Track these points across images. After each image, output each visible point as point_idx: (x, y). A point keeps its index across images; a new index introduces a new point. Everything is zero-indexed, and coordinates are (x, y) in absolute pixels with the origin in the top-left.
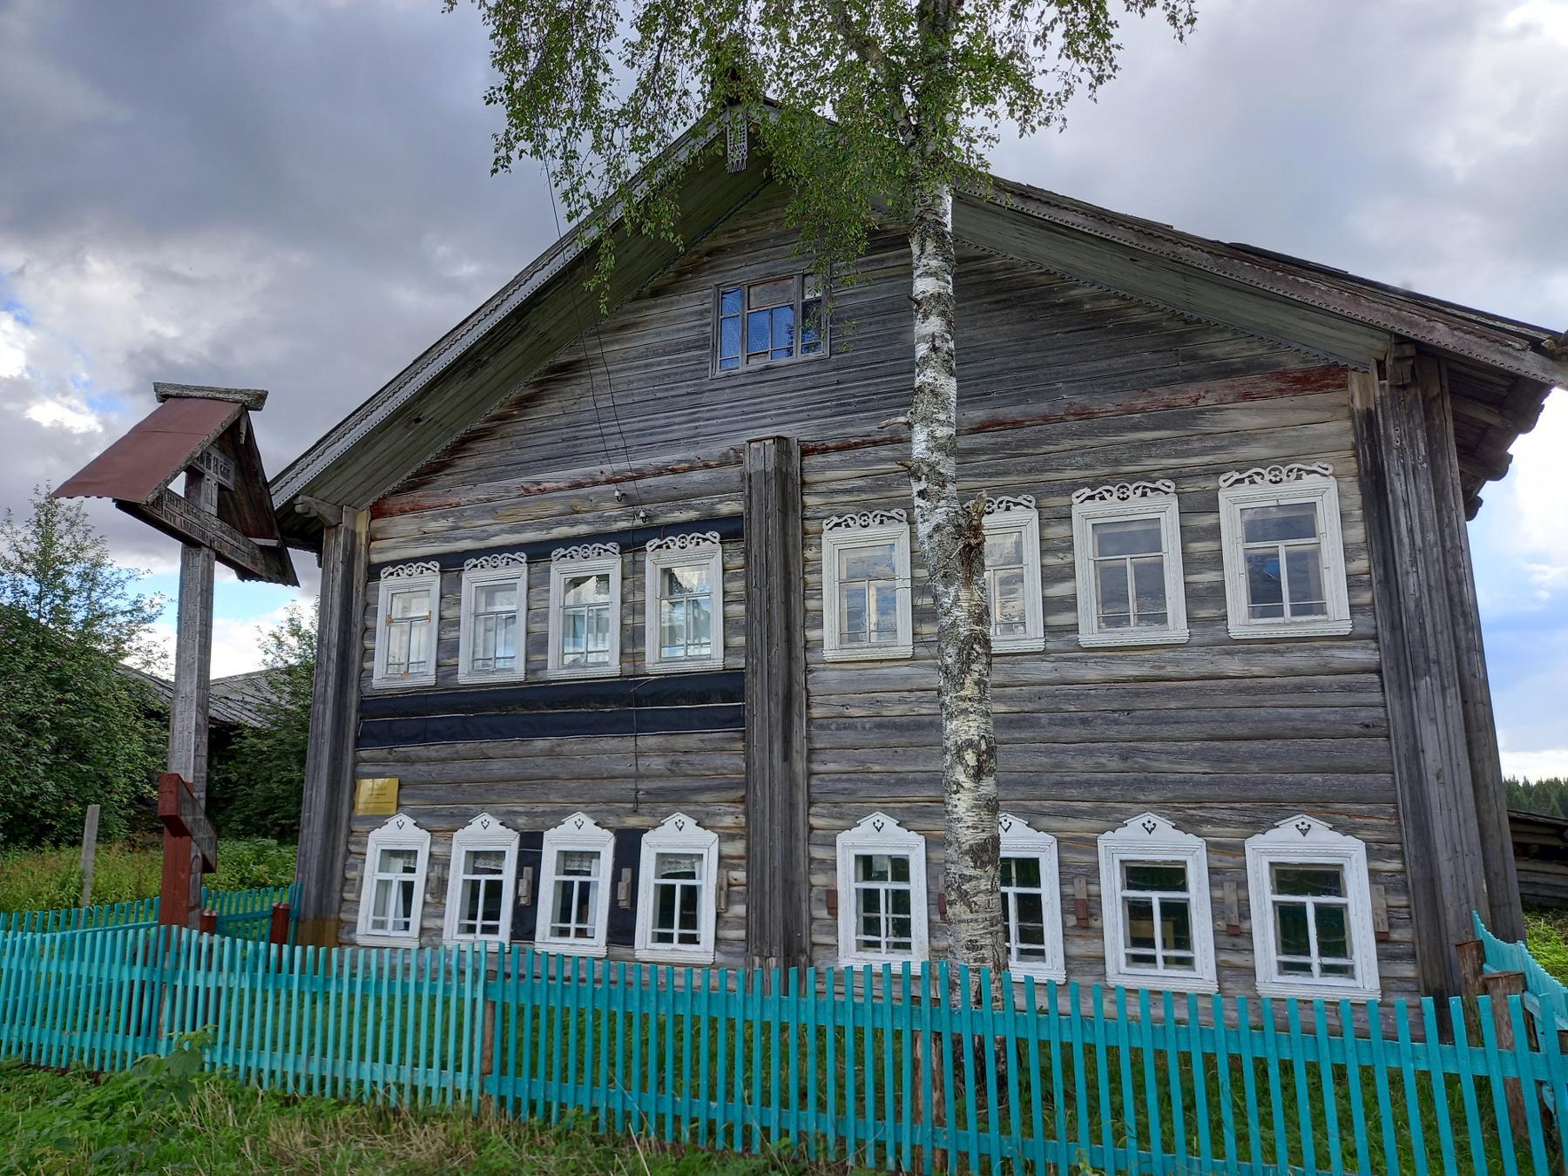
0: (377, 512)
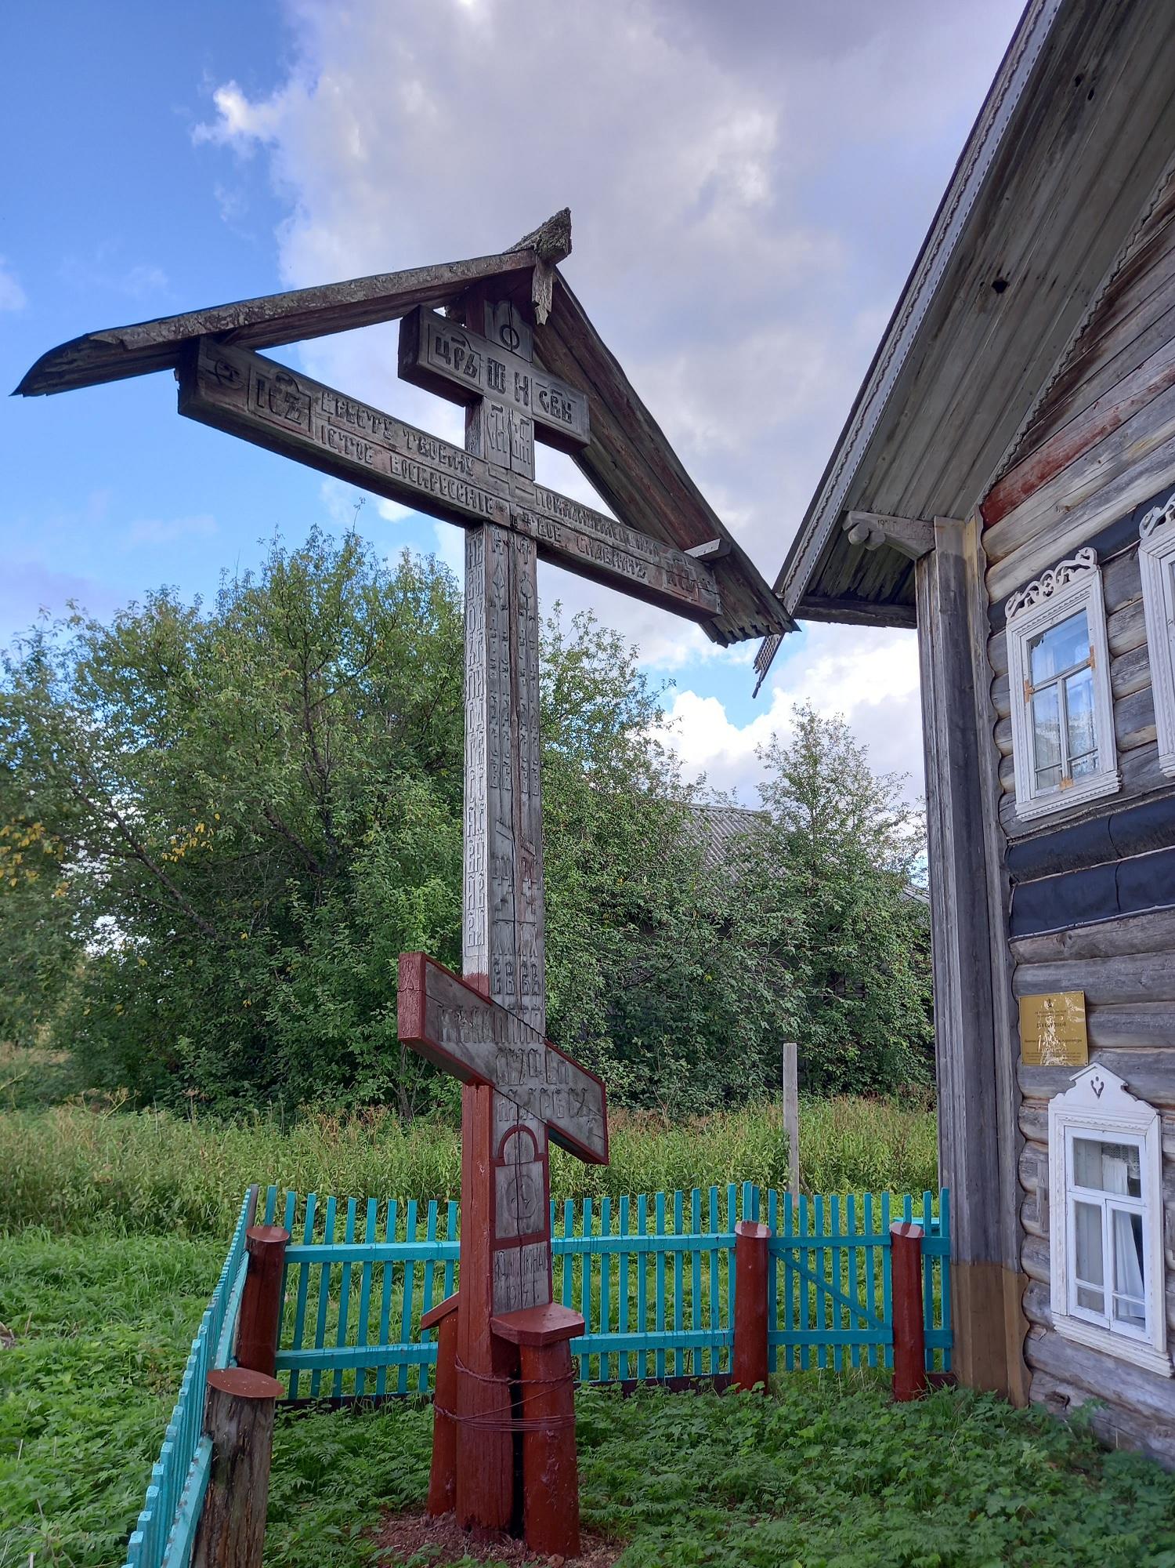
0: (993, 511)
